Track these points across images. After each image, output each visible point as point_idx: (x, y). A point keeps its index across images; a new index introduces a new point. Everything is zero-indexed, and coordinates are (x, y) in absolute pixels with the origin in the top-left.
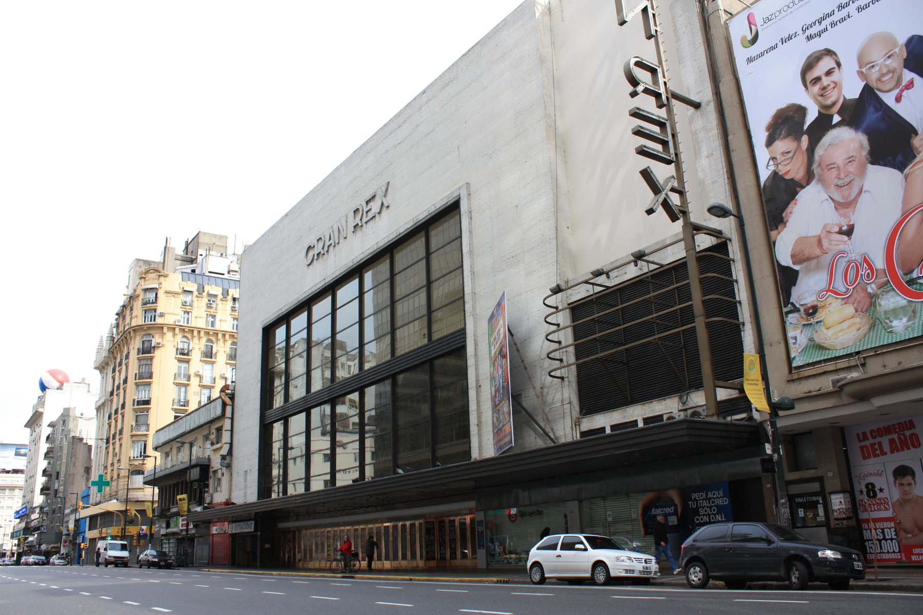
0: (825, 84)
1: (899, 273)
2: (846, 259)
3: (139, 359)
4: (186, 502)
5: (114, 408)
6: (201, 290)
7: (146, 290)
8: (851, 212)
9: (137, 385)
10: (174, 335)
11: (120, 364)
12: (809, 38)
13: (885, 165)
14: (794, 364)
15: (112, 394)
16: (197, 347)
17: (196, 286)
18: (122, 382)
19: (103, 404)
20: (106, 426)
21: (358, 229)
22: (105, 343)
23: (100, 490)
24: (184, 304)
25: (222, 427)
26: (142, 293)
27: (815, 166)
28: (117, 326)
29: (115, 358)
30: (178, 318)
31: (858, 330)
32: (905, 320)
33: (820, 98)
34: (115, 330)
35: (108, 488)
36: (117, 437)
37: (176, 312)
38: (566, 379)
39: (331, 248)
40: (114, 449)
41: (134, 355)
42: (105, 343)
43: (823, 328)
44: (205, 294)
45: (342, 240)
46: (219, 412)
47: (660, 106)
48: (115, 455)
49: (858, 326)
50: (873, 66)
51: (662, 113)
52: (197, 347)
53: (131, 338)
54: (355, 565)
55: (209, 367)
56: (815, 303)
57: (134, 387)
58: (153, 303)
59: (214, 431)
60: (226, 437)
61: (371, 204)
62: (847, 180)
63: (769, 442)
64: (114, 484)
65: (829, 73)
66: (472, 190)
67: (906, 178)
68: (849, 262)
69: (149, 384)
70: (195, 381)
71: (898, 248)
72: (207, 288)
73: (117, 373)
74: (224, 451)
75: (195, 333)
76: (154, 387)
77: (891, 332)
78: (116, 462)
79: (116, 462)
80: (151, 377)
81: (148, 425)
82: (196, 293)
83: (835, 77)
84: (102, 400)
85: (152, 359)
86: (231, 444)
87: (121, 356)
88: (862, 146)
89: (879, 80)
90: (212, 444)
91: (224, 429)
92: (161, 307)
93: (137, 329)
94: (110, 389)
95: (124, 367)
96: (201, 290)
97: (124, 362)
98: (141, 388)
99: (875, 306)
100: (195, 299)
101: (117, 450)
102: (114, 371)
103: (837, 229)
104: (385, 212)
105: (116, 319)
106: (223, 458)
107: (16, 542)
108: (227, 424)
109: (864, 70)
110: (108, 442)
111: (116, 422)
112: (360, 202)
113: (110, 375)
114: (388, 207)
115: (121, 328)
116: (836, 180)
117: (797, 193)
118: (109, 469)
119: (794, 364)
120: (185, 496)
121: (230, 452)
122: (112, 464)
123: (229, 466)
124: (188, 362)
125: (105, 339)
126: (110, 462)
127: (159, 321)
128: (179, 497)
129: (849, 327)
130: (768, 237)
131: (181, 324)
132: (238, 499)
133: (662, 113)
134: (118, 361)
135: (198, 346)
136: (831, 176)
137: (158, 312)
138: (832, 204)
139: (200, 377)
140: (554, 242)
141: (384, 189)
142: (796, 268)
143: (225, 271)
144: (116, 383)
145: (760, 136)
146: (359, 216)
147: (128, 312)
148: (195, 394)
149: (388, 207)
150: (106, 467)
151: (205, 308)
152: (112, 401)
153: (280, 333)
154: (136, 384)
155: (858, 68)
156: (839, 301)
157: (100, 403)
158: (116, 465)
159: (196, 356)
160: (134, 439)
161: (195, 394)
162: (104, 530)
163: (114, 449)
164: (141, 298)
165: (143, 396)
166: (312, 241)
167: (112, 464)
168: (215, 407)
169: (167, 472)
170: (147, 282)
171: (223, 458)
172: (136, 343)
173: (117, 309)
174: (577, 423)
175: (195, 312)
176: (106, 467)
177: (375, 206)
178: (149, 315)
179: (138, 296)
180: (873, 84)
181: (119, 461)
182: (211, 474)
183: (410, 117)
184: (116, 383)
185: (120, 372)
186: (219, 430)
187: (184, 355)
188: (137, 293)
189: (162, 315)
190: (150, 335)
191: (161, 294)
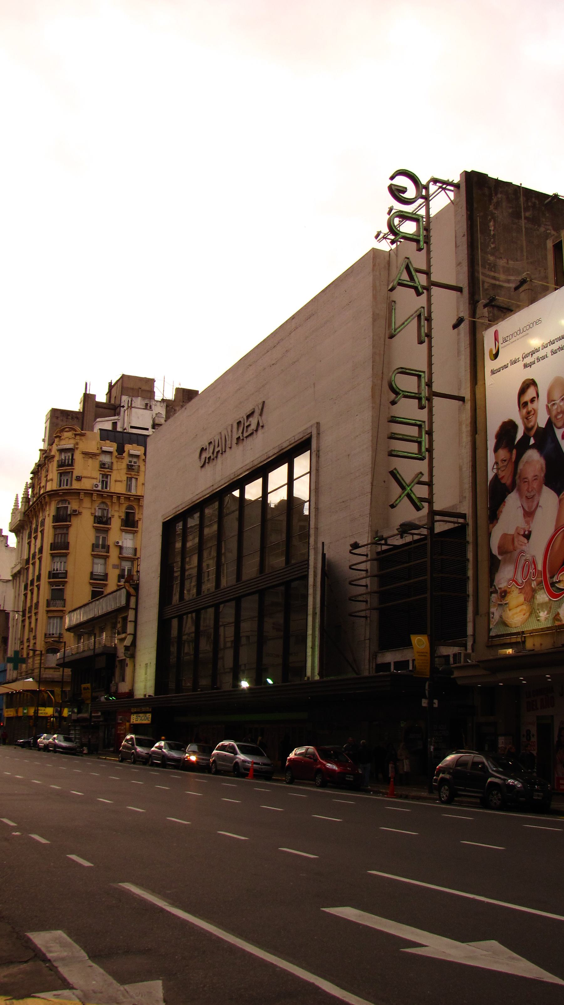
0: (530, 409)
1: (548, 576)
2: (524, 558)
3: (55, 528)
4: (90, 691)
5: (30, 578)
6: (121, 450)
7: (61, 451)
8: (536, 520)
9: (53, 556)
10: (92, 501)
11: (36, 531)
12: (525, 366)
13: (551, 488)
14: (491, 634)
15: (27, 561)
16: (116, 515)
17: (115, 445)
18: (37, 551)
19: (19, 572)
20: (22, 597)
21: (241, 441)
22: (20, 505)
23: (15, 668)
24: (103, 465)
25: (127, 617)
26: (57, 454)
27: (517, 477)
28: (33, 486)
29: (31, 523)
30: (95, 482)
31: (524, 615)
32: (546, 612)
33: (525, 420)
34: (30, 490)
35: (24, 666)
36: (33, 611)
37: (93, 476)
38: (368, 619)
39: (220, 455)
40: (30, 623)
41: (49, 523)
42: (20, 505)
43: (508, 609)
44: (125, 455)
45: (228, 449)
46: (123, 602)
47: (421, 407)
48: (31, 630)
49: (524, 612)
50: (554, 404)
51: (423, 415)
52: (116, 515)
53: (46, 503)
54: (495, 803)
55: (130, 536)
56: (506, 588)
57: (49, 557)
58: (69, 465)
59: (120, 620)
60: (130, 628)
61: (251, 419)
62: (532, 494)
63: (425, 698)
64: (30, 661)
65: (532, 401)
66: (322, 429)
67: (560, 501)
68: (526, 560)
69: (66, 555)
70: (114, 553)
71: (550, 555)
72: (127, 447)
73: (33, 540)
74: (128, 642)
75: (115, 500)
76: (71, 558)
77: (538, 620)
78: (31, 638)
79: (31, 638)
80: (67, 548)
81: (64, 600)
82: (115, 454)
83: (535, 405)
84: (18, 568)
85: (68, 527)
86: (135, 635)
87: (37, 521)
88: (542, 468)
89: (556, 416)
90: (119, 634)
91: (129, 619)
92: (78, 470)
93: (53, 494)
94: (25, 557)
95: (39, 534)
96: (121, 450)
97: (39, 530)
98: (57, 559)
99: (534, 599)
100: (114, 460)
101: (33, 625)
102: (30, 537)
103: (522, 533)
104: (260, 432)
105: (32, 479)
106: (127, 648)
107: (163, 954)
108: (131, 615)
109: (549, 405)
110: (24, 615)
111: (32, 593)
112: (241, 414)
113: (26, 541)
114: (263, 426)
115: (36, 490)
116: (526, 492)
117: (506, 497)
118: (26, 645)
119: (491, 634)
120: (88, 685)
121: (134, 643)
122: (28, 640)
123: (133, 657)
124: (107, 531)
125: (20, 500)
126: (26, 637)
127: (76, 485)
128: (83, 686)
129: (520, 611)
130: (488, 529)
131: (99, 488)
132: (40, 712)
133: (423, 415)
134: (34, 526)
135: (117, 516)
136: (525, 487)
137: (76, 473)
138: (522, 512)
139: (121, 548)
140: (370, 496)
141: (260, 407)
142: (500, 558)
143: (149, 425)
144: (32, 552)
145: (491, 442)
146: (240, 431)
147: (43, 473)
148: (115, 567)
149: (263, 426)
150: (22, 643)
151: (124, 471)
152: (27, 569)
153: (180, 526)
154: (51, 554)
155: (546, 403)
156: (518, 590)
157: (15, 570)
158: (32, 642)
159: (116, 524)
160: (50, 615)
161: (115, 567)
162: (21, 710)
163: (30, 623)
164: (56, 459)
165: (58, 566)
166: (205, 444)
167: (28, 640)
168: (120, 596)
169: (77, 656)
170: (63, 442)
171: (127, 648)
172: (51, 511)
173: (32, 467)
174: (374, 656)
175: (115, 476)
176: (22, 643)
177: (253, 421)
178: (64, 478)
179: (53, 457)
180: (553, 420)
181: (35, 637)
182: (117, 663)
183: (282, 340)
184: (32, 552)
185: (36, 538)
186: (125, 619)
187: (102, 523)
188: (53, 453)
189: (79, 479)
190: (65, 501)
191: (78, 456)
